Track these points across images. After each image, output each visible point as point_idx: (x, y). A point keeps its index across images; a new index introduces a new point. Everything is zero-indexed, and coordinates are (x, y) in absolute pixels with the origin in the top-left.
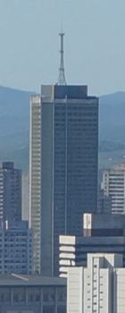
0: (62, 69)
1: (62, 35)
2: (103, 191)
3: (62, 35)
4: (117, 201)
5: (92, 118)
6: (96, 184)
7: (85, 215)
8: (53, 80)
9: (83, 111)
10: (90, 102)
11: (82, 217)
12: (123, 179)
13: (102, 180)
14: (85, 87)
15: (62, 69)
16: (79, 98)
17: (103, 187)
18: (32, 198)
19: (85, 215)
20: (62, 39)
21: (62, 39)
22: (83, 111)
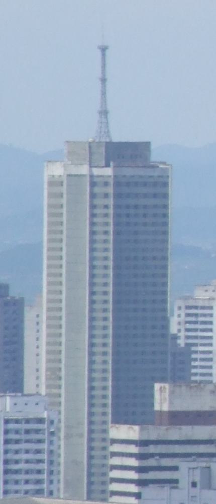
0: (104, 113)
1: (104, 49)
2: (175, 337)
3: (104, 49)
4: (199, 356)
5: (151, 202)
6: (166, 327)
7: (157, 386)
8: (88, 132)
9: (144, 190)
10: (156, 173)
11: (152, 388)
12: (211, 315)
13: (173, 315)
14: (147, 145)
15: (104, 113)
16: (203, 299)
17: (174, 329)
18: (48, 318)
19: (157, 386)
20: (104, 55)
21: (104, 55)
22: (144, 190)
